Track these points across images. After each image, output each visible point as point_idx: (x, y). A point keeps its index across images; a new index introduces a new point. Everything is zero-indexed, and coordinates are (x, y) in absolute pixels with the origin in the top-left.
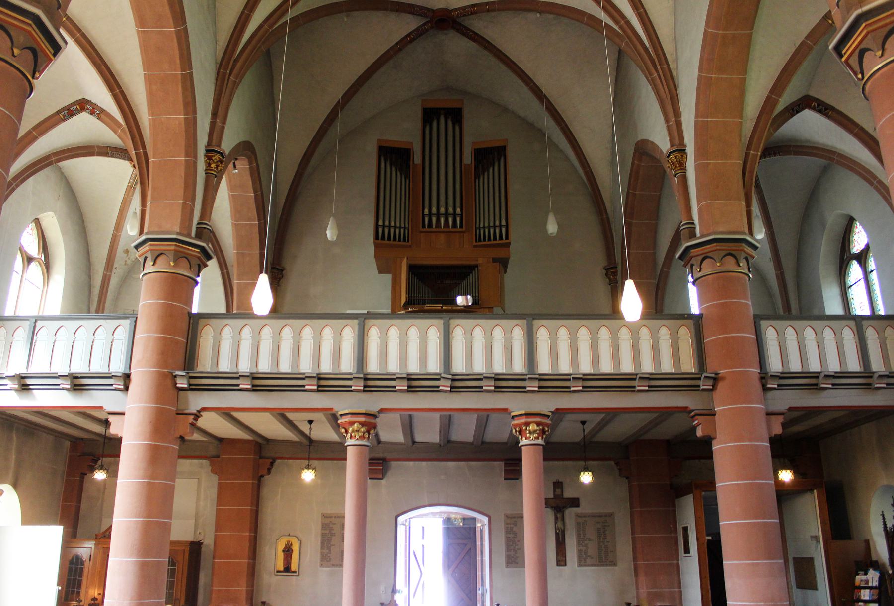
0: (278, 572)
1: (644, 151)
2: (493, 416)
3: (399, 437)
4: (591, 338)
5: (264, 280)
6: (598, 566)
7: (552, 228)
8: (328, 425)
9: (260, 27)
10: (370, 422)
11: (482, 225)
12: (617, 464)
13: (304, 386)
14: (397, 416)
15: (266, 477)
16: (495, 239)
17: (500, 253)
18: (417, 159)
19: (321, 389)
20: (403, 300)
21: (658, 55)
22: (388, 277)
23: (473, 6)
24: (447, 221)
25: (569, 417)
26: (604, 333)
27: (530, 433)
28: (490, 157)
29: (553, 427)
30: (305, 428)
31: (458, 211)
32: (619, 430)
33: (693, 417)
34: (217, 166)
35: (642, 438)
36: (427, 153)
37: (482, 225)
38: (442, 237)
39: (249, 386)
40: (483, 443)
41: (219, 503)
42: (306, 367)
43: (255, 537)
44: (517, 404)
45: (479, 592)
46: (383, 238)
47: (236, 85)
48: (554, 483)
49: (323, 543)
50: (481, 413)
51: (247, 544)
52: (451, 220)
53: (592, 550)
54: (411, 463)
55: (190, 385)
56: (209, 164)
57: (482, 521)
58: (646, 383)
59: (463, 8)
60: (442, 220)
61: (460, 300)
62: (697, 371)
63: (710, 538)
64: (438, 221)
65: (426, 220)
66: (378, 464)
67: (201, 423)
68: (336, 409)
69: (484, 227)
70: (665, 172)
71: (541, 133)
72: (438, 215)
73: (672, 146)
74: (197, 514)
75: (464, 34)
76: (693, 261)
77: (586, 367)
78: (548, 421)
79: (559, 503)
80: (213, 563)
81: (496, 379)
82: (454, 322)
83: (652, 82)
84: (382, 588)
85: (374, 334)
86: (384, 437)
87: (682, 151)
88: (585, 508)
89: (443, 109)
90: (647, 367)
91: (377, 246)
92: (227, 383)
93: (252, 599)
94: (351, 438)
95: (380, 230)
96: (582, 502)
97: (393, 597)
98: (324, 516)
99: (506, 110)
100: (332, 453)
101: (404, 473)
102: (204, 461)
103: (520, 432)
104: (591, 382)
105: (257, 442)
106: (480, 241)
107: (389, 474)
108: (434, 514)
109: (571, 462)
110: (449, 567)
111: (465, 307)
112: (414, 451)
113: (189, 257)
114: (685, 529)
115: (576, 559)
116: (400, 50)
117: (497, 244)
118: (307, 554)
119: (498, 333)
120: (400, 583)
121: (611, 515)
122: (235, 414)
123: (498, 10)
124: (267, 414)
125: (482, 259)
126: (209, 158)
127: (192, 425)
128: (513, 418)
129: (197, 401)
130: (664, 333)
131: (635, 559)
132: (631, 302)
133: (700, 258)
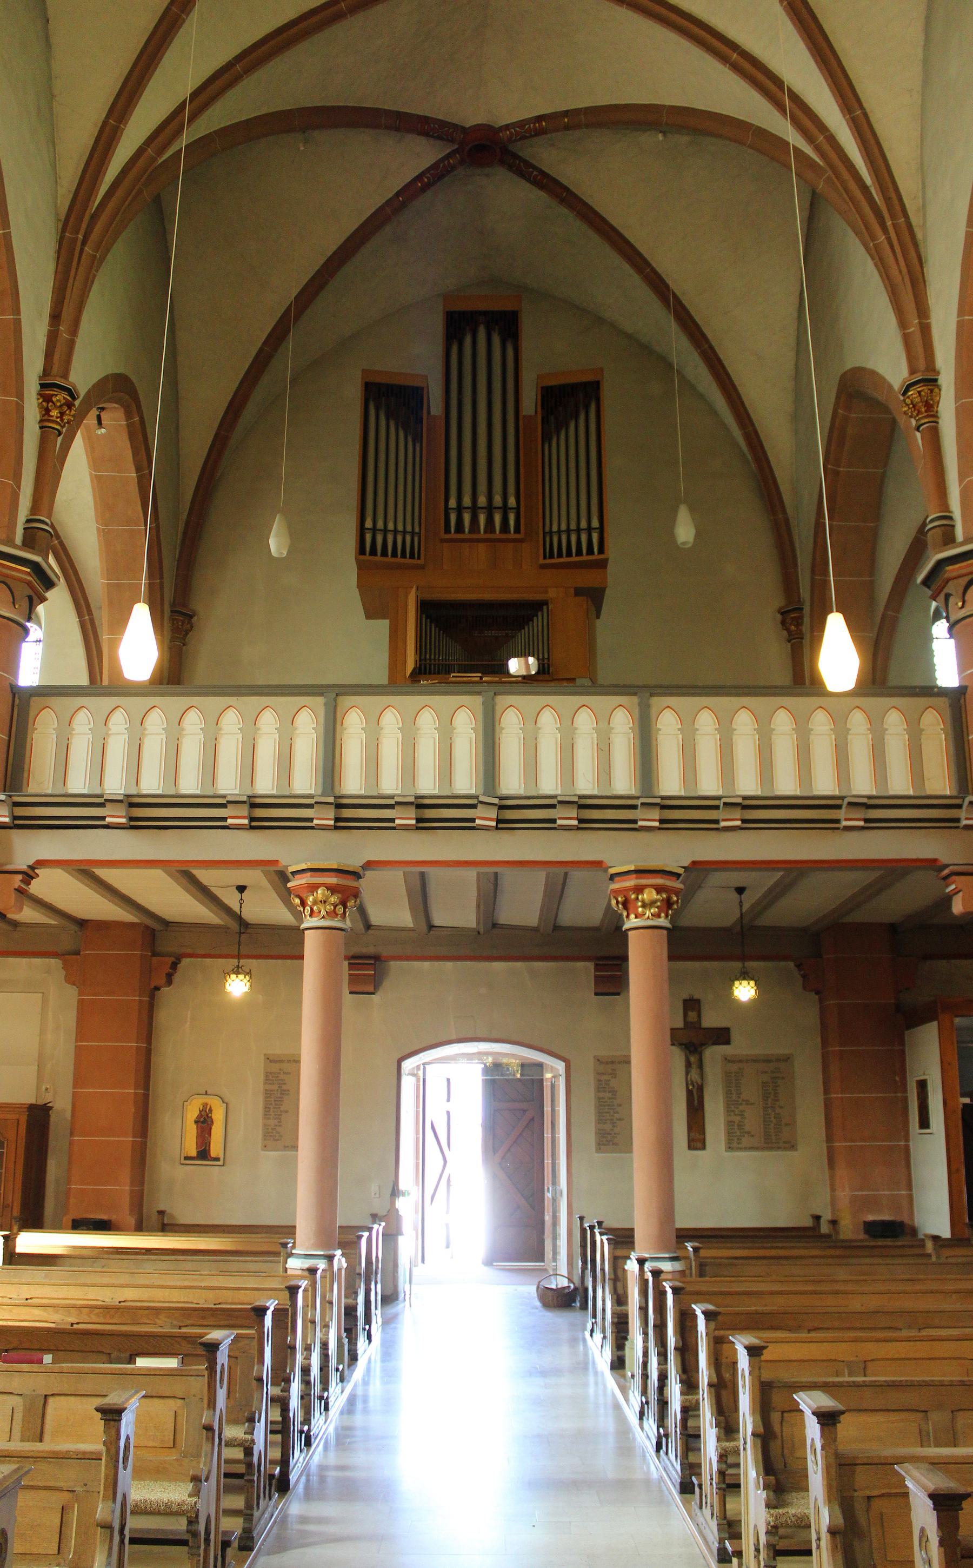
0: (186, 1158)
1: (856, 390)
2: (576, 875)
3: (403, 917)
4: (758, 731)
5: (141, 614)
6: (763, 1149)
7: (685, 532)
8: (275, 895)
9: (140, 152)
10: (346, 886)
11: (555, 528)
12: (798, 966)
13: (225, 819)
14: (398, 875)
15: (165, 990)
16: (579, 552)
17: (588, 578)
18: (435, 406)
19: (255, 824)
20: (410, 666)
21: (887, 200)
22: (385, 624)
23: (539, 118)
24: (490, 520)
25: (717, 878)
26: (782, 722)
27: (644, 906)
28: (570, 401)
29: (687, 895)
30: (231, 899)
31: (512, 501)
32: (806, 904)
33: (945, 878)
34: (62, 414)
35: (848, 919)
36: (454, 402)
37: (555, 528)
38: (482, 548)
39: (123, 820)
40: (556, 928)
41: (81, 1033)
42: (229, 784)
43: (146, 1097)
44: (619, 853)
45: (548, 1195)
46: (373, 552)
47: (96, 263)
48: (685, 1001)
49: (267, 1109)
50: (552, 870)
51: (131, 1109)
52: (497, 518)
53: (752, 1119)
54: (426, 964)
55: (15, 818)
56: (47, 411)
57: (554, 1070)
58: (862, 813)
59: (521, 124)
60: (482, 519)
61: (515, 666)
62: (955, 793)
63: (967, 1100)
64: (474, 520)
65: (453, 518)
66: (365, 965)
67: (35, 888)
68: (283, 862)
69: (559, 532)
70: (894, 422)
71: (664, 365)
72: (474, 509)
73: (912, 371)
74: (41, 1055)
75: (521, 174)
76: (950, 588)
77: (748, 784)
78: (678, 885)
79: (694, 1037)
80: (71, 1143)
81: (582, 807)
82: (503, 701)
83: (877, 255)
84: (374, 1187)
85: (354, 723)
86: (377, 916)
87: (932, 382)
88: (740, 1046)
89: (485, 313)
90: (863, 784)
91: (361, 567)
92: (84, 814)
93: (141, 1205)
94: (311, 915)
95: (368, 537)
96: (735, 1036)
97: (393, 1203)
98: (269, 1059)
99: (599, 320)
100: (280, 945)
101: (410, 981)
102: (53, 961)
103: (625, 904)
104: (758, 812)
105: (147, 927)
106: (552, 556)
107: (386, 984)
108: (470, 1057)
109: (715, 964)
110: (495, 1151)
111: (524, 677)
112: (433, 942)
113: (9, 581)
114: (922, 1085)
115: (722, 1137)
116: (404, 205)
117: (583, 561)
118: (239, 1125)
119: (585, 720)
120: (406, 1178)
121: (787, 1059)
122: (101, 873)
123: (588, 126)
124: (158, 873)
125: (556, 589)
126: (46, 399)
127: (20, 891)
128: (612, 877)
129: (30, 848)
130: (894, 721)
131: (829, 1138)
132: (839, 656)
133: (963, 581)
